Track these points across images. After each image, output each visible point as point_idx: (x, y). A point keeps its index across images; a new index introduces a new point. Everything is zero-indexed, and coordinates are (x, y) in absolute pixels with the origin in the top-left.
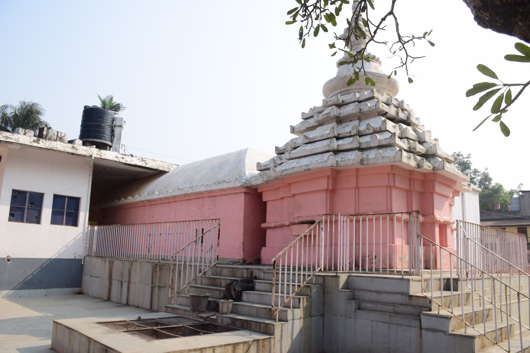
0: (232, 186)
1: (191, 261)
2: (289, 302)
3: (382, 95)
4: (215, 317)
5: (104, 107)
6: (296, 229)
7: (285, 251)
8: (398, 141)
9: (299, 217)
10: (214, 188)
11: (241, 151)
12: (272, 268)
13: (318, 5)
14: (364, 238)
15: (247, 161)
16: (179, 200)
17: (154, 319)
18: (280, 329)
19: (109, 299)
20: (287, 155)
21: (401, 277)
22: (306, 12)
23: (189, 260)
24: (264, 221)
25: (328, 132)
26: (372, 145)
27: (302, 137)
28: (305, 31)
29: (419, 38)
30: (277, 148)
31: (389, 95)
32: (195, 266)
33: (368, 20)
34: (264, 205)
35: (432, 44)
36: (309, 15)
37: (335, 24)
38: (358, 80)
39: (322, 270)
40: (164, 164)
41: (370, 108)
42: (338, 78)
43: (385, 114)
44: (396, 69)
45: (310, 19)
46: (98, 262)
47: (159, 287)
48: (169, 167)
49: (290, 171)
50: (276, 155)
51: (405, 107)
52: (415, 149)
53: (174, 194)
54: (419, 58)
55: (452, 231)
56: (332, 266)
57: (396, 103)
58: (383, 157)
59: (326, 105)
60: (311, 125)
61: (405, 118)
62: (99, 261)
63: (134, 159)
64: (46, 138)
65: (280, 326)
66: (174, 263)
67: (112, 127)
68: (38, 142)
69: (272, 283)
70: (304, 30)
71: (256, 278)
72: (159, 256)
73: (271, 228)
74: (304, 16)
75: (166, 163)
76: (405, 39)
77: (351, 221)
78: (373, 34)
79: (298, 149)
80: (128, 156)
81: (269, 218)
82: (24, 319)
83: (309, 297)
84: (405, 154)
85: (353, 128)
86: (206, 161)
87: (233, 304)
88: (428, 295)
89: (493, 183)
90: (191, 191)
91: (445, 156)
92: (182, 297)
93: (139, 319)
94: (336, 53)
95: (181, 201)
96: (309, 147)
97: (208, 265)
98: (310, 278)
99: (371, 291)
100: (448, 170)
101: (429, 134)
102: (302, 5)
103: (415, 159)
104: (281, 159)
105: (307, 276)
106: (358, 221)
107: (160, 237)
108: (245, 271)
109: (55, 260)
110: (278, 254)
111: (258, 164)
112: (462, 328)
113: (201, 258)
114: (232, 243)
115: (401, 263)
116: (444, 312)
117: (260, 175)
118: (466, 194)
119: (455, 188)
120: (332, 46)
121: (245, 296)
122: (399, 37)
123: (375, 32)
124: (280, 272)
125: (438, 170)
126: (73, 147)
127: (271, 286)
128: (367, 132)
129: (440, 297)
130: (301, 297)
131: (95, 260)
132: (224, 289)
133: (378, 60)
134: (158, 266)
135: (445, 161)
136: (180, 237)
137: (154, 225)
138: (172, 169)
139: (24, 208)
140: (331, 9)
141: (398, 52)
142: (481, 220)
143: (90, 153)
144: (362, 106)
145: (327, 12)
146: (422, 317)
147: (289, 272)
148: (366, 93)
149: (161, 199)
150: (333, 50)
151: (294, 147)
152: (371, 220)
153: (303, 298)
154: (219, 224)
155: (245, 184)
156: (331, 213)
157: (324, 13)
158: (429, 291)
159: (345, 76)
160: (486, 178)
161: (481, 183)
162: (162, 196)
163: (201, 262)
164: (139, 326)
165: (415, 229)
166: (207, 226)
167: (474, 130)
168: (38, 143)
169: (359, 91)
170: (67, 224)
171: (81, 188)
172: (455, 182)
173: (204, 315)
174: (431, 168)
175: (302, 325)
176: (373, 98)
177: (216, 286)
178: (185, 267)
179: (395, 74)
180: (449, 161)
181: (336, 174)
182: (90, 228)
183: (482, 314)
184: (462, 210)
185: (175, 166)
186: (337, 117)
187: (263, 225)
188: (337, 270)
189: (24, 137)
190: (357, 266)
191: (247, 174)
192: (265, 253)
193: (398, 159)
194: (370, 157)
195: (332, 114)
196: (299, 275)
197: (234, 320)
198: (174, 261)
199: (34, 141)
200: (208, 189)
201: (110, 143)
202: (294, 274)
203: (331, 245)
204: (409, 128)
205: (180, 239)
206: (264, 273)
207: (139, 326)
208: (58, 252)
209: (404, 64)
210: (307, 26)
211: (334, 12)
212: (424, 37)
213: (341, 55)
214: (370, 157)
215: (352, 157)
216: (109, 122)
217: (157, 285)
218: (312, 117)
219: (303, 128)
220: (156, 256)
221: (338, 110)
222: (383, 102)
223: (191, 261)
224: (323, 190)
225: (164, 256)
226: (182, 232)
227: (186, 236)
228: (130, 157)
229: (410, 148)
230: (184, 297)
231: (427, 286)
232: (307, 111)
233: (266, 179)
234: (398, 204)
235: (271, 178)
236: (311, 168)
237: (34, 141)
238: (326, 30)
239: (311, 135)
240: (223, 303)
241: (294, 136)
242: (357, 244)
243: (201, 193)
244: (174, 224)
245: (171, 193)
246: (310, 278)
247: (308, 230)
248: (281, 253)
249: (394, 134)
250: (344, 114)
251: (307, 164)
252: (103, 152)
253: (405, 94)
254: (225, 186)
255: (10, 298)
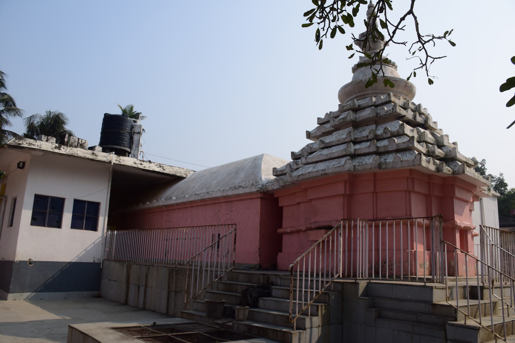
0: (248, 192)
1: (207, 266)
2: (307, 309)
3: (399, 99)
4: (230, 324)
5: (123, 115)
6: (313, 235)
7: (307, 261)
8: (416, 145)
9: (315, 222)
10: (230, 193)
11: (257, 157)
12: (290, 273)
13: (335, 6)
14: (384, 244)
15: (263, 166)
16: (196, 205)
17: (169, 325)
18: (297, 338)
19: (126, 303)
20: (303, 160)
21: (423, 284)
22: (323, 13)
23: (204, 265)
24: (281, 226)
25: (344, 136)
26: (390, 149)
27: (318, 142)
28: (322, 33)
29: (439, 38)
30: (293, 154)
31: (405, 99)
32: (211, 271)
33: (386, 20)
34: (281, 210)
35: (453, 44)
36: (326, 16)
37: (352, 25)
38: (376, 82)
39: (341, 276)
40: (182, 170)
41: (387, 111)
42: (354, 83)
43: (401, 117)
44: (415, 71)
45: (327, 20)
46: (115, 266)
47: (176, 292)
48: (186, 173)
49: (307, 176)
50: (292, 160)
51: (422, 111)
52: (434, 152)
53: (191, 199)
54: (440, 58)
55: (473, 236)
56: (351, 272)
57: (413, 107)
58: (401, 161)
59: (342, 109)
60: (327, 130)
61: (423, 122)
62: (117, 264)
63: (152, 165)
64: (67, 145)
65: (298, 334)
66: (190, 267)
67: (131, 133)
68: (59, 148)
69: (289, 290)
70: (320, 32)
71: (272, 284)
72: (175, 260)
73: (287, 233)
74: (320, 18)
75: (183, 169)
76: (426, 39)
77: (370, 226)
78: (392, 35)
79: (314, 154)
80: (146, 162)
81: (285, 224)
82: (42, 322)
83: (328, 304)
84: (424, 158)
85: (370, 132)
86: (223, 167)
87: (250, 311)
88: (453, 303)
89: (509, 188)
90: (207, 196)
91: (465, 160)
92: (198, 302)
93: (154, 325)
94: (353, 54)
95: (198, 206)
96: (326, 152)
97: (224, 270)
98: (328, 285)
99: (391, 299)
100: (469, 174)
101: (446, 138)
102: (319, 7)
103: (434, 163)
104: (297, 164)
105: (325, 283)
106: (377, 227)
107: (177, 242)
108: (261, 277)
109: (75, 263)
110: (294, 260)
111: (274, 169)
112: (491, 340)
113: (217, 263)
114: (248, 245)
115: (422, 272)
116: (471, 322)
117: (276, 180)
118: (485, 200)
119: (475, 193)
120: (350, 48)
121: (261, 302)
122: (419, 36)
123: (394, 33)
124: (298, 278)
125: (458, 174)
126: (93, 153)
127: (289, 293)
128: (385, 136)
129: (465, 306)
130: (320, 304)
131: (113, 263)
132: (240, 295)
133: (394, 65)
134: (174, 271)
135: (465, 165)
136: (196, 242)
137: (171, 230)
138: (189, 175)
139: (46, 213)
140: (349, 10)
141: (418, 53)
142: (500, 226)
143: (110, 159)
144: (379, 110)
145: (345, 13)
146: (447, 326)
147: (306, 278)
148: (382, 98)
149: (178, 204)
150: (351, 52)
151: (309, 152)
152: (391, 225)
153: (322, 306)
154: (236, 230)
155: (261, 189)
156: (349, 218)
157: (341, 14)
158: (452, 299)
159: (361, 81)
160: (501, 184)
161: (496, 188)
162: (179, 201)
163: (217, 267)
164: (154, 333)
165: (436, 236)
166: (223, 232)
167: (508, 128)
168: (60, 150)
169: (375, 95)
170: (87, 229)
171: (100, 194)
172: (475, 186)
173: (220, 322)
174: (451, 172)
175: (320, 334)
176: (390, 102)
177: (232, 292)
178: (201, 272)
179: (415, 76)
180: (469, 166)
181: (353, 179)
182: (109, 232)
183: (511, 325)
184: (481, 215)
185: (192, 172)
186: (353, 121)
187: (280, 231)
188: (356, 276)
189: (47, 144)
190: (377, 273)
191: (263, 178)
192: (281, 257)
193: (418, 163)
194: (388, 161)
195: (348, 119)
196: (317, 281)
197: (251, 327)
198: (190, 265)
199: (56, 147)
200: (224, 194)
201: (129, 150)
202: (312, 281)
203: (349, 251)
204: (427, 132)
205: (196, 244)
206: (281, 279)
207: (154, 333)
208: (78, 256)
209: (424, 65)
210: (323, 28)
211: (351, 13)
212: (445, 37)
213: (356, 60)
214: (388, 161)
215: (369, 161)
216: (128, 129)
217: (173, 289)
218: (328, 122)
219: (318, 134)
220: (173, 260)
221: (354, 115)
222: (400, 106)
223: (207, 266)
224: (341, 195)
225: (181, 261)
226: (198, 237)
227: (202, 241)
228: (148, 163)
229: (428, 151)
230: (200, 302)
231: (451, 294)
232: (323, 117)
233: (282, 184)
234: (417, 209)
235: (287, 183)
236: (328, 172)
237: (56, 147)
238: (343, 31)
239: (328, 139)
240: (239, 309)
241: (310, 142)
242: (377, 250)
243: (217, 198)
244: (190, 229)
245: (188, 198)
246: (328, 285)
247: (325, 236)
248: (298, 259)
249: (413, 137)
250: (361, 119)
251: (324, 168)
252: (122, 158)
253: (423, 97)
254: (241, 191)
255: (31, 300)
